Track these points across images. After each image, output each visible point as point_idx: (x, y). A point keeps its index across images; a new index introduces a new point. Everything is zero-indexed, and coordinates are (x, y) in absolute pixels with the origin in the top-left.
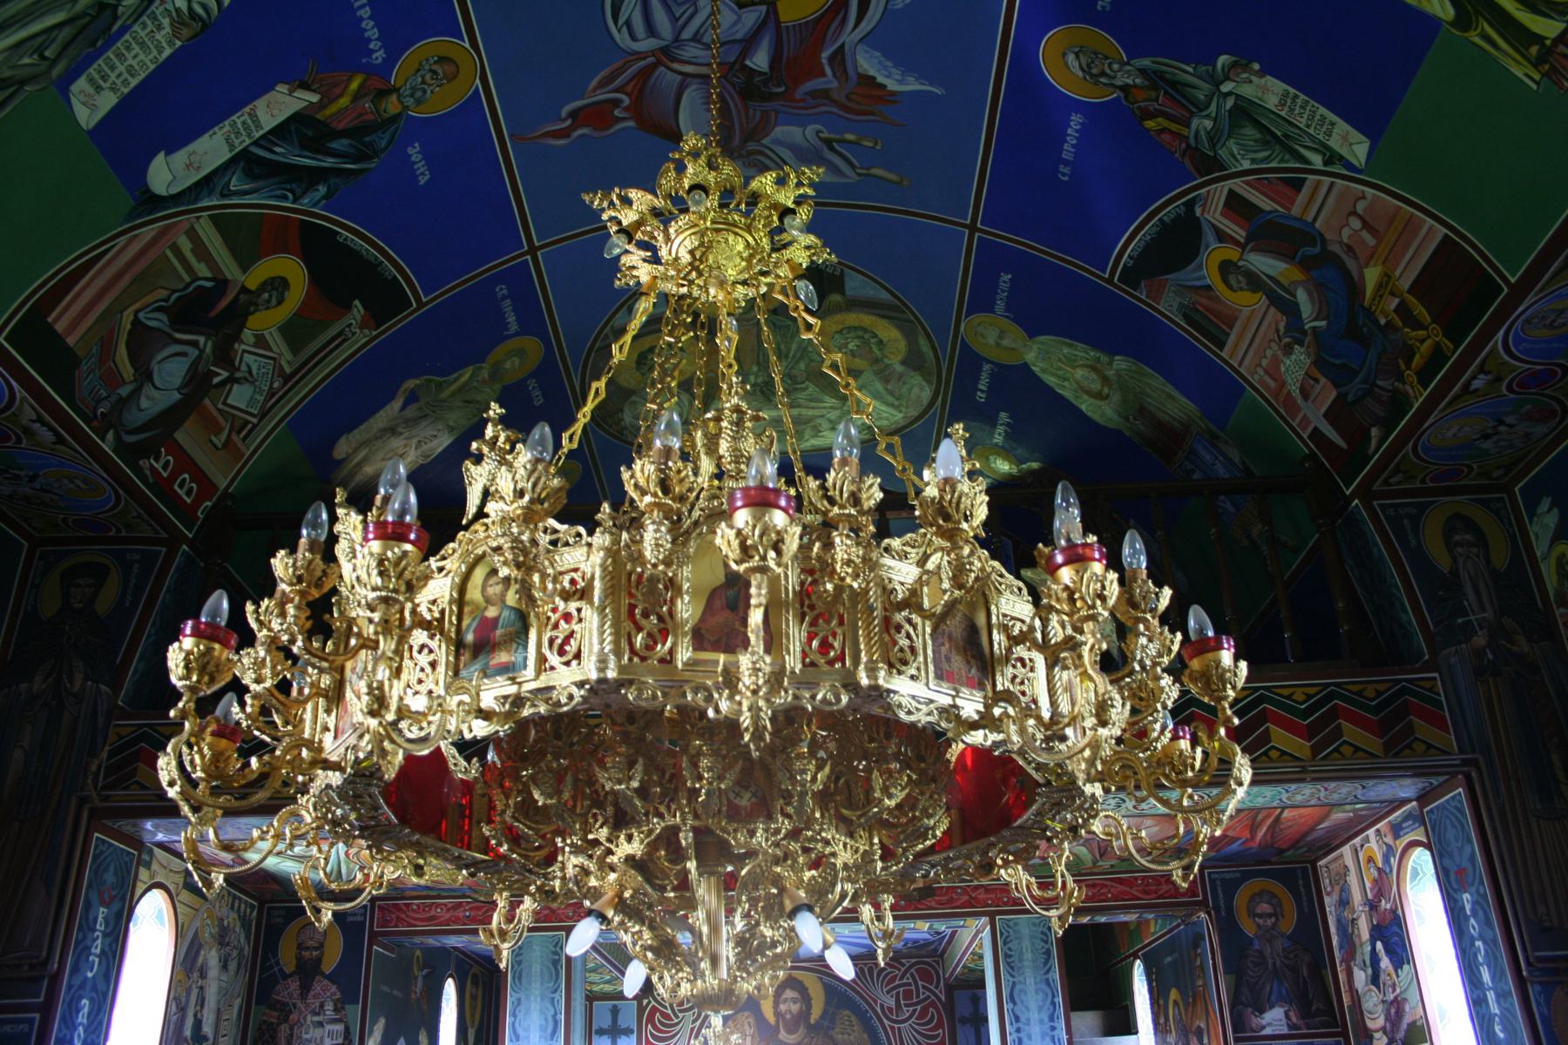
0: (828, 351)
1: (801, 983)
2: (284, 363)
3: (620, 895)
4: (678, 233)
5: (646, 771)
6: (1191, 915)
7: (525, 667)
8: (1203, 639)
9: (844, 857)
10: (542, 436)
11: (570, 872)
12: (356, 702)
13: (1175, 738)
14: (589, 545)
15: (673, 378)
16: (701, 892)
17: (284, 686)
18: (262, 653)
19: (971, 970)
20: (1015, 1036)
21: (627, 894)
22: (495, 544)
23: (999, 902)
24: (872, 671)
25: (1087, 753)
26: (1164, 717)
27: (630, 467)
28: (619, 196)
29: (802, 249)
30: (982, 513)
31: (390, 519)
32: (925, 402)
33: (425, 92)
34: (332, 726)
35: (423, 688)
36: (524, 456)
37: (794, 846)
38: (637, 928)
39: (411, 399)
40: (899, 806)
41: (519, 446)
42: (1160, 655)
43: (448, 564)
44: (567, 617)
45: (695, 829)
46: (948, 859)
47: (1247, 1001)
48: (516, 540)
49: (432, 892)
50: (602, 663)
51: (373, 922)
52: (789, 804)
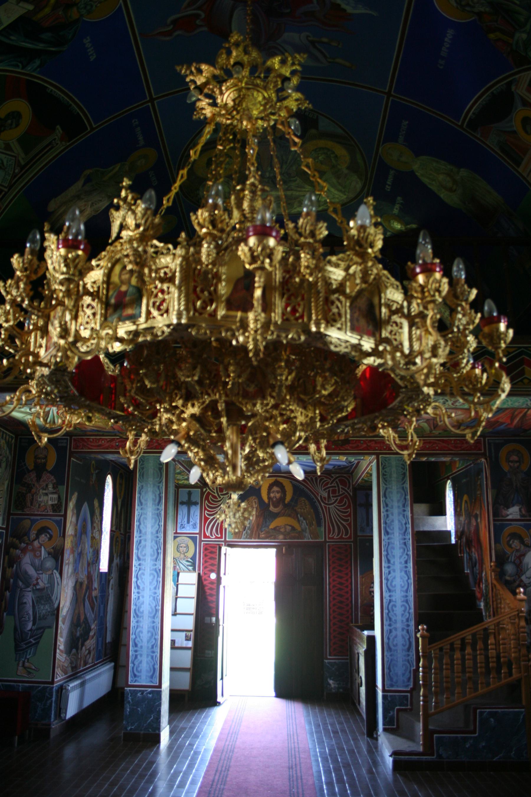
0: (305, 157)
1: (281, 484)
2: (20, 159)
3: (188, 433)
4: (227, 89)
5: (202, 372)
6: (477, 460)
7: (140, 316)
8: (491, 316)
9: (300, 419)
10: (151, 197)
11: (164, 421)
12: (55, 330)
13: (473, 367)
14: (174, 255)
15: (221, 168)
16: (228, 433)
17: (21, 325)
18: (8, 307)
19: (366, 481)
20: (385, 513)
21: (191, 433)
22: (125, 253)
23: (379, 447)
24: (318, 325)
25: (425, 371)
26: (468, 357)
27: (195, 213)
28: (196, 68)
29: (294, 101)
30: (379, 244)
31: (70, 237)
32: (358, 190)
33: (92, 6)
34: (44, 345)
35: (89, 326)
36: (141, 207)
37: (275, 412)
38: (196, 450)
39: (88, 180)
40: (330, 395)
41: (139, 202)
42: (468, 324)
43: (102, 263)
44: (162, 291)
45: (226, 402)
46: (354, 424)
47: (501, 502)
48: (135, 250)
49: (99, 432)
50: (179, 315)
51: (68, 444)
52: (273, 391)
